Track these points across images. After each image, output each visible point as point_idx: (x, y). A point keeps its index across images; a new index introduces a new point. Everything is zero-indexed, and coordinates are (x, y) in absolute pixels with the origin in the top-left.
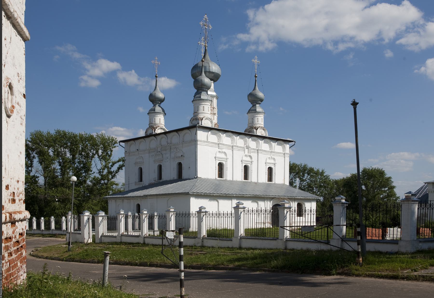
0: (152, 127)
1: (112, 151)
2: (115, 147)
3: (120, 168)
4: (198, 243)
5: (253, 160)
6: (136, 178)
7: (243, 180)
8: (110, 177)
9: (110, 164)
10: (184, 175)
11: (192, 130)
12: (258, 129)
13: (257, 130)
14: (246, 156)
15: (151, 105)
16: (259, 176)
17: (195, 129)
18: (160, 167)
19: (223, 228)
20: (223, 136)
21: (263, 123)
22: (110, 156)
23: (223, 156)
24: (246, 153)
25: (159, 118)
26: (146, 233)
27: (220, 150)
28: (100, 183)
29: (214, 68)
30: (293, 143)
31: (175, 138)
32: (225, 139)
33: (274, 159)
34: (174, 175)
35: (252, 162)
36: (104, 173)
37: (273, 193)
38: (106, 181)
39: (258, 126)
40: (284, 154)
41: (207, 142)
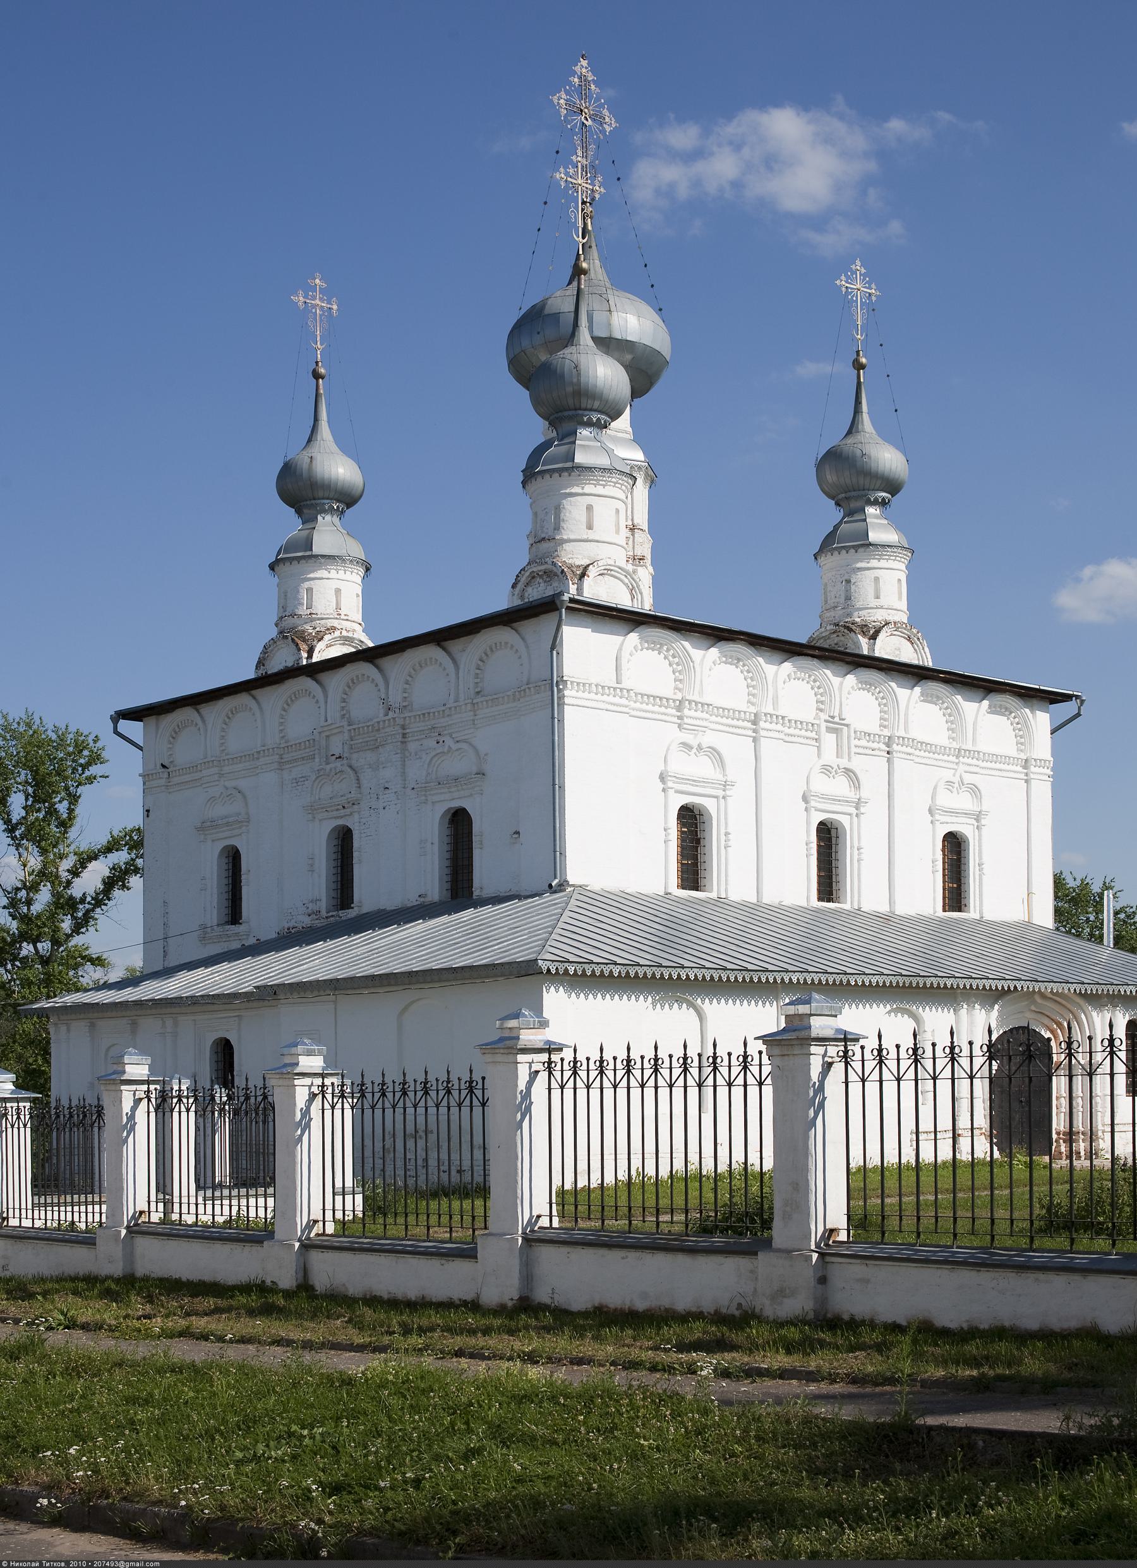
0: (292, 632)
1: (74, 799)
2: (91, 780)
3: (116, 880)
4: (781, 1293)
5: (865, 793)
6: (208, 903)
7: (815, 903)
8: (66, 925)
9: (66, 865)
10: (484, 878)
11: (529, 627)
12: (882, 636)
13: (874, 637)
14: (827, 769)
15: (289, 524)
16: (895, 881)
17: (546, 623)
18: (343, 841)
19: (708, 1167)
20: (708, 659)
21: (903, 605)
22: (65, 825)
23: (703, 768)
24: (829, 755)
25: (334, 584)
26: (142, 1205)
27: (688, 738)
28: (15, 958)
29: (634, 321)
30: (1070, 708)
31: (428, 679)
32: (717, 672)
33: (975, 790)
34: (429, 879)
35: (858, 804)
36: (36, 908)
37: (993, 968)
38: (44, 947)
39: (879, 616)
40: (1026, 764)
41: (618, 689)
